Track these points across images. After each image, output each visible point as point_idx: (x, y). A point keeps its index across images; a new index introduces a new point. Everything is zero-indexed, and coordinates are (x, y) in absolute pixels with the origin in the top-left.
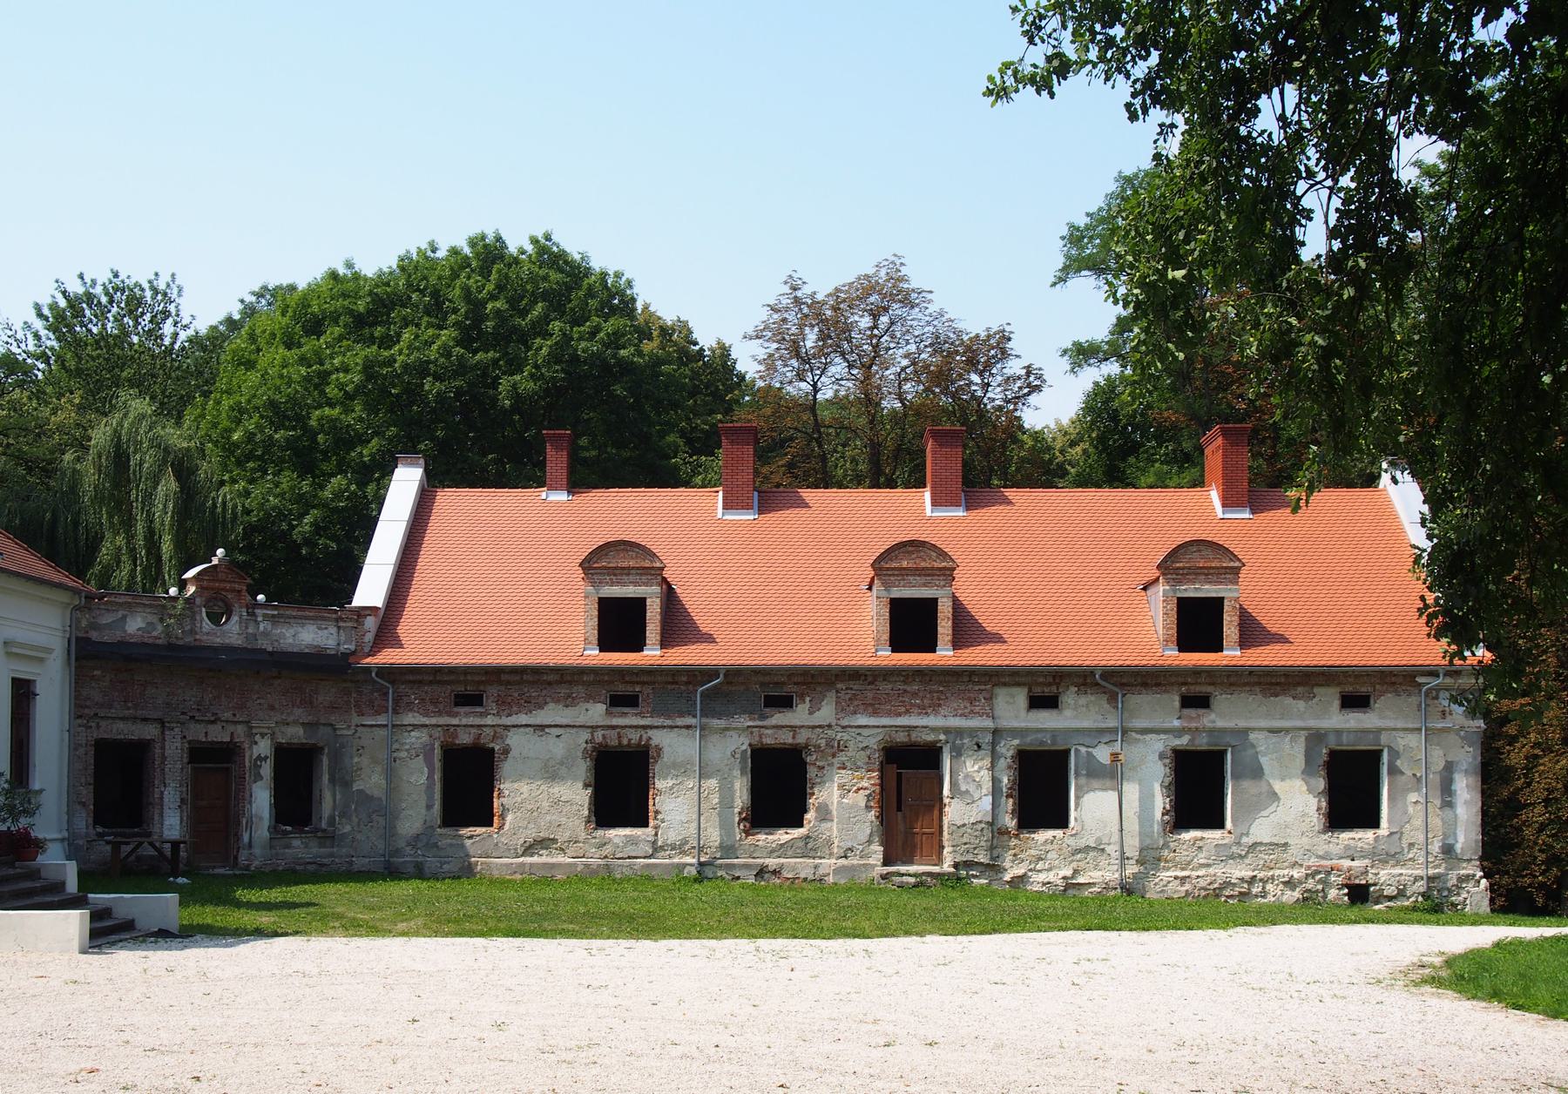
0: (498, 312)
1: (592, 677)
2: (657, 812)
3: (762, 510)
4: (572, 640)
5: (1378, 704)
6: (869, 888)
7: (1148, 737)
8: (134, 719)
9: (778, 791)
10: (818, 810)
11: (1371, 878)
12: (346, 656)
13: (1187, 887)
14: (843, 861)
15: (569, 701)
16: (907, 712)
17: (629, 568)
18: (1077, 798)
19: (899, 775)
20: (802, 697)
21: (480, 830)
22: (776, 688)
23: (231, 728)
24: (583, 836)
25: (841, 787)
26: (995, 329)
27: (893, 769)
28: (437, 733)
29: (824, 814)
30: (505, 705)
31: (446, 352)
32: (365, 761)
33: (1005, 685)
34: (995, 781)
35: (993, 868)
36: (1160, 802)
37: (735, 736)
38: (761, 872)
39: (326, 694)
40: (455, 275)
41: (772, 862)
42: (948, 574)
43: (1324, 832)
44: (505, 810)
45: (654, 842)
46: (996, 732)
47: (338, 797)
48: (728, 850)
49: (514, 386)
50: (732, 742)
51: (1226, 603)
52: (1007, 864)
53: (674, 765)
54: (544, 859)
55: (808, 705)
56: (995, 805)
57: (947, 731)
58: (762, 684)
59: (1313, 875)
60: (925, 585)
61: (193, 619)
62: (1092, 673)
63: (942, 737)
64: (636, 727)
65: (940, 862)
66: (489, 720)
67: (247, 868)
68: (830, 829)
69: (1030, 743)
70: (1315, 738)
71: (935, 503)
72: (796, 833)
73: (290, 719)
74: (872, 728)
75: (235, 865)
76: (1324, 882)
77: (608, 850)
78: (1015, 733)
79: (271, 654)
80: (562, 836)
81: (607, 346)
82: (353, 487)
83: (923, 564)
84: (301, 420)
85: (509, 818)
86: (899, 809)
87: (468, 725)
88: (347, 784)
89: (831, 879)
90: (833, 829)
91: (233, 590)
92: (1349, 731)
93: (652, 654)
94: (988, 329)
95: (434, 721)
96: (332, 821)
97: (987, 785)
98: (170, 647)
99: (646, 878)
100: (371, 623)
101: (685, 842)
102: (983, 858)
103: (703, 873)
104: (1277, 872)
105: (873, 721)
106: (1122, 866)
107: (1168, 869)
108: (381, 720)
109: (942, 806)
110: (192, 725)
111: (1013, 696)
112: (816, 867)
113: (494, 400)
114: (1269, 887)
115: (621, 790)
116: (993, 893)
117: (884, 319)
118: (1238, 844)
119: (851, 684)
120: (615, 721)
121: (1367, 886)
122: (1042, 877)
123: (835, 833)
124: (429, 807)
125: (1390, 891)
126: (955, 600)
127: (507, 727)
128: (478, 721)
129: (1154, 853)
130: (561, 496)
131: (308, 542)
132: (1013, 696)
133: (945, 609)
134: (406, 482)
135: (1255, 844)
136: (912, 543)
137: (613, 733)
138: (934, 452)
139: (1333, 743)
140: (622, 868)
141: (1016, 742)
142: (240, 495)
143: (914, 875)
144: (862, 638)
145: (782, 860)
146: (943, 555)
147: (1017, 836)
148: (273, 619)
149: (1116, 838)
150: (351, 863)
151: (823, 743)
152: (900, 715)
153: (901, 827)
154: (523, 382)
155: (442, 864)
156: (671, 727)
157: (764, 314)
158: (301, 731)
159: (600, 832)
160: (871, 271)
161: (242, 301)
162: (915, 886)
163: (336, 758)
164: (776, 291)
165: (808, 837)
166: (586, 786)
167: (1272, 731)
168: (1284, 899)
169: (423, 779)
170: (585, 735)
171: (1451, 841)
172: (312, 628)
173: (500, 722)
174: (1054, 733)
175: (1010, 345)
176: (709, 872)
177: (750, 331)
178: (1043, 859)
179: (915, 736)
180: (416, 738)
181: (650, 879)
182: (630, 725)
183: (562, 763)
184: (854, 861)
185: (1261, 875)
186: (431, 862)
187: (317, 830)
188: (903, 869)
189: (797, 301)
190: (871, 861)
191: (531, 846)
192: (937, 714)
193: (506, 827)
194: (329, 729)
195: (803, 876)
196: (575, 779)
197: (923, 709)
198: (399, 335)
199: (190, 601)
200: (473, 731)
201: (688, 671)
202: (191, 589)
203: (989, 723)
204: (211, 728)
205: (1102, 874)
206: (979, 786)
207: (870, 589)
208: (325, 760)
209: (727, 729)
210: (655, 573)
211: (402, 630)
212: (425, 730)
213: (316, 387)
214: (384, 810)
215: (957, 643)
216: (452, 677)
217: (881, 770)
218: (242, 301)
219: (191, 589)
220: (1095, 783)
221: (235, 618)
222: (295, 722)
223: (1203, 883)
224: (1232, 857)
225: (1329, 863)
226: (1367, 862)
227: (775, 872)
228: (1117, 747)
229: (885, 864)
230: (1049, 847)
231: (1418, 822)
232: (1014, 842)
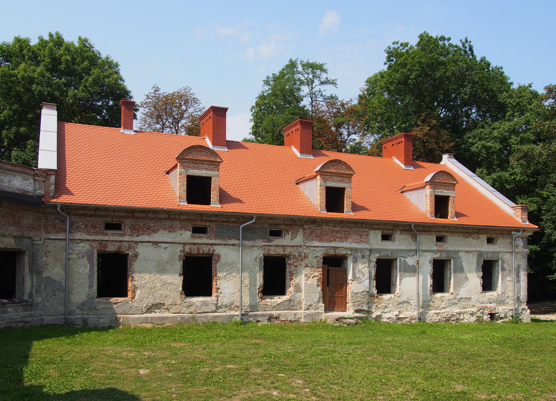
0: (67, 61)
1: (186, 217)
2: (218, 289)
7: (426, 253)
9: (275, 279)
10: (295, 287)
11: (497, 311)
12: (40, 197)
14: (307, 311)
15: (171, 229)
16: (335, 240)
17: (203, 161)
18: (400, 280)
19: (328, 270)
20: (288, 231)
24: (179, 302)
28: (95, 244)
29: (298, 289)
30: (135, 230)
32: (50, 260)
33: (374, 229)
34: (370, 272)
36: (430, 281)
37: (257, 250)
38: (270, 318)
39: (28, 219)
41: (275, 313)
43: (482, 293)
45: (217, 304)
46: (371, 250)
47: (35, 281)
48: (254, 307)
50: (254, 253)
51: (451, 198)
52: (373, 310)
53: (227, 264)
55: (290, 235)
57: (351, 249)
58: (270, 224)
60: (340, 181)
63: (349, 252)
64: (207, 244)
66: (126, 238)
68: (300, 296)
69: (383, 255)
70: (480, 254)
73: (7, 233)
74: (320, 247)
77: (192, 309)
78: (378, 251)
80: (168, 302)
83: (340, 172)
85: (138, 292)
87: (113, 241)
88: (39, 273)
89: (302, 320)
92: (490, 252)
95: (93, 237)
96: (31, 295)
97: (367, 275)
99: (211, 325)
101: (232, 303)
102: (365, 308)
104: (468, 310)
105: (320, 244)
107: (432, 310)
108: (61, 236)
111: (376, 234)
112: (295, 314)
118: (455, 298)
119: (311, 226)
120: (196, 241)
123: (303, 297)
124: (91, 287)
127: (136, 242)
128: (120, 238)
129: (427, 303)
132: (376, 234)
134: (49, 118)
135: (461, 298)
137: (195, 247)
141: (377, 255)
144: (172, 193)
145: (280, 312)
146: (349, 168)
147: (377, 297)
150: (42, 319)
151: (297, 254)
152: (331, 241)
155: (99, 319)
156: (225, 245)
158: (13, 241)
162: (356, 324)
163: (33, 257)
165: (290, 300)
166: (180, 275)
167: (467, 252)
169: (87, 271)
170: (180, 248)
171: (519, 295)
173: (132, 239)
174: (392, 251)
180: (83, 247)
182: (204, 244)
183: (167, 263)
184: (312, 311)
186: (92, 319)
187: (21, 301)
190: (319, 311)
191: (150, 308)
192: (346, 241)
193: (136, 297)
194: (29, 241)
195: (289, 319)
196: (174, 273)
197: (341, 240)
200: (117, 244)
201: (236, 216)
203: (367, 246)
208: (26, 259)
209: (253, 246)
211: (69, 184)
212: (88, 243)
214: (65, 289)
216: (106, 213)
220: (407, 274)
222: (9, 235)
223: (445, 315)
224: (453, 304)
225: (483, 305)
227: (277, 318)
230: (389, 302)
232: (376, 300)
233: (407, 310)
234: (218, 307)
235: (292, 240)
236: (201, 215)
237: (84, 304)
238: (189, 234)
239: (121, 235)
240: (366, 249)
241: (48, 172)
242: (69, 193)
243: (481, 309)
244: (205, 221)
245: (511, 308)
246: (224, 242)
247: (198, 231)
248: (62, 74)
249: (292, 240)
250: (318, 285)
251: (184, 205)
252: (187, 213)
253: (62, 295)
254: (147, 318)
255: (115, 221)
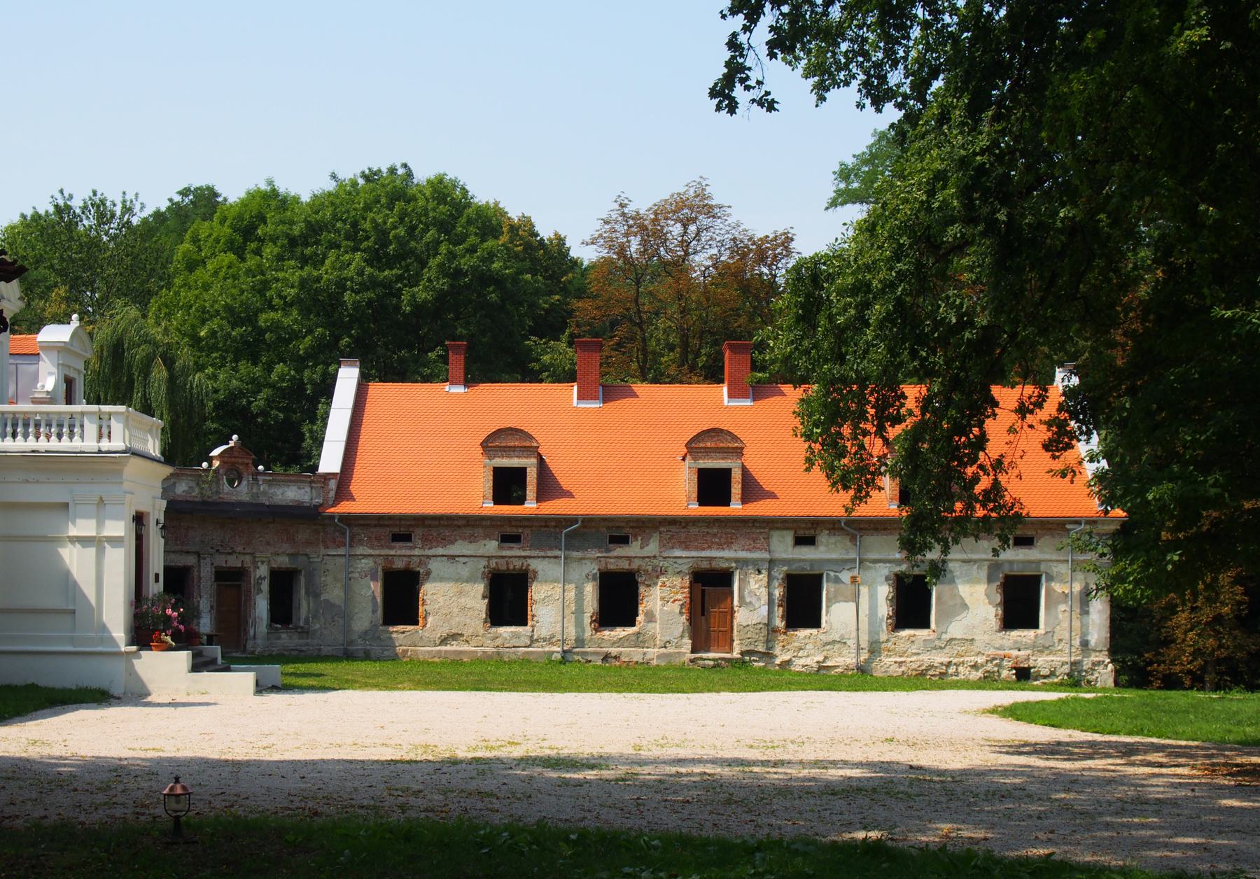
3: (606, 399)
4: (476, 497)
5: (1039, 543)
6: (682, 668)
8: (181, 552)
9: (618, 601)
11: (1031, 663)
12: (317, 507)
13: (903, 668)
14: (663, 650)
15: (472, 539)
16: (709, 547)
18: (828, 607)
19: (703, 591)
20: (636, 537)
21: (409, 628)
22: (618, 531)
23: (242, 557)
24: (481, 632)
25: (662, 599)
26: (781, 231)
27: (699, 586)
28: (379, 560)
29: (650, 617)
30: (428, 541)
31: (361, 273)
32: (329, 579)
33: (778, 529)
34: (770, 595)
35: (768, 655)
36: (884, 610)
38: (606, 657)
39: (303, 534)
40: (368, 208)
41: (614, 651)
42: (739, 452)
43: (1000, 631)
44: (427, 613)
48: (580, 642)
49: (413, 296)
54: (455, 648)
56: (770, 612)
57: (737, 560)
58: (608, 528)
59: (992, 660)
61: (218, 483)
62: (839, 521)
63: (734, 565)
65: (731, 650)
66: (417, 552)
67: (253, 652)
69: (795, 569)
71: (731, 396)
72: (630, 630)
74: (687, 556)
75: (244, 651)
76: (998, 665)
78: (784, 562)
79: (268, 506)
80: (467, 632)
81: (483, 260)
82: (293, 373)
84: (251, 319)
85: (430, 619)
86: (703, 614)
87: (401, 555)
88: (317, 596)
89: (655, 662)
90: (656, 628)
91: (243, 464)
92: (1018, 562)
93: (531, 506)
94: (775, 232)
95: (377, 552)
96: (307, 621)
97: (765, 598)
98: (204, 503)
100: (333, 484)
102: (761, 648)
103: (566, 657)
104: (966, 659)
105: (684, 554)
106: (858, 653)
108: (341, 551)
109: (732, 612)
110: (217, 556)
113: (397, 308)
114: (961, 669)
115: (507, 600)
116: (767, 672)
117: (692, 228)
119: (670, 528)
120: (505, 553)
121: (1029, 668)
122: (802, 661)
124: (374, 612)
125: (1045, 672)
126: (744, 469)
127: (429, 557)
128: (408, 552)
130: (459, 389)
131: (263, 413)
132: (783, 537)
133: (736, 475)
134: (347, 378)
135: (951, 640)
136: (714, 430)
137: (503, 561)
138: (731, 359)
139: (1007, 570)
140: (509, 654)
142: (209, 378)
143: (713, 660)
144: (677, 494)
147: (785, 633)
148: (269, 483)
149: (854, 634)
150: (320, 650)
151: (650, 568)
153: (704, 627)
154: (422, 293)
157: (598, 225)
159: (494, 630)
160: (681, 190)
161: (171, 200)
162: (714, 667)
164: (607, 208)
167: (964, 561)
168: (971, 677)
170: (484, 562)
172: (295, 488)
174: (812, 562)
175: (793, 245)
176: (569, 657)
177: (587, 239)
178: (803, 648)
179: (715, 565)
180: (366, 564)
181: (529, 661)
184: (671, 650)
185: (955, 660)
186: (376, 649)
187: (296, 627)
188: (704, 655)
189: (623, 214)
190: (683, 650)
192: (729, 548)
194: (305, 558)
197: (720, 546)
198: (325, 257)
199: (216, 471)
202: (216, 464)
203: (766, 555)
204: (229, 558)
205: (845, 659)
206: (759, 599)
207: (684, 459)
208: (302, 579)
210: (534, 451)
211: (355, 487)
213: (259, 292)
214: (344, 614)
215: (745, 500)
217: (691, 587)
218: (171, 200)
219: (216, 464)
221: (244, 483)
222: (283, 553)
223: (914, 666)
224: (935, 648)
225: (1002, 652)
226: (1029, 652)
227: (615, 657)
228: (855, 572)
229: (693, 652)
231: (1066, 624)
232: (782, 637)
233: (840, 655)
234: (533, 641)
235: (642, 548)
236: (509, 520)
237: (366, 632)
238: (495, 544)
239: (411, 548)
240: (762, 560)
241: (328, 477)
242: (352, 498)
243: (994, 659)
244: (516, 526)
245: (1065, 659)
246: (542, 554)
247: (509, 539)
248: (390, 263)
249: (642, 548)
250: (681, 613)
251: (490, 508)
252: (491, 519)
253: (342, 622)
254: (440, 652)
255: (403, 531)
